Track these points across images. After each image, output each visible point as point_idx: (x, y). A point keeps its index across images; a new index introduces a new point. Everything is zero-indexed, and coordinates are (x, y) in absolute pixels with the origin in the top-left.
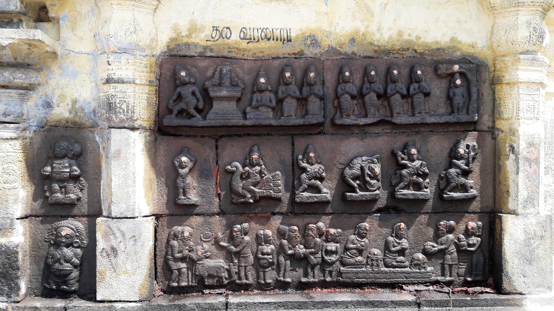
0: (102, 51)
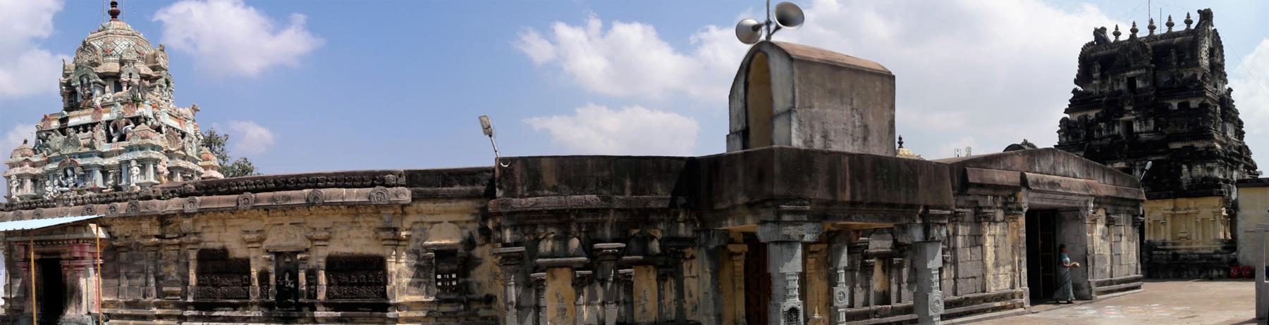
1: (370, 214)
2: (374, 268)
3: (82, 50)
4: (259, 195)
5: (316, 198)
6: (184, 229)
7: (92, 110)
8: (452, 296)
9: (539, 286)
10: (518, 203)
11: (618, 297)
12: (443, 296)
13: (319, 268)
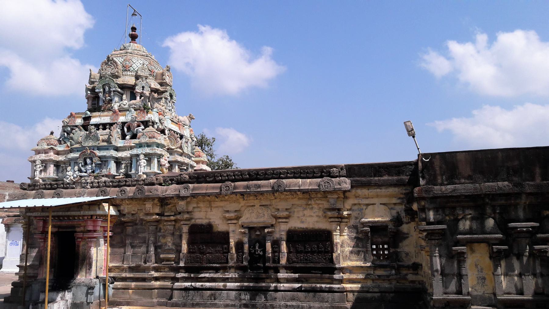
0: (280, 231)
1: (320, 199)
2: (322, 240)
3: (107, 64)
4: (236, 183)
5: (279, 186)
6: (179, 209)
7: (111, 113)
8: (385, 263)
9: (460, 258)
10: (437, 189)
11: (534, 269)
12: (378, 263)
13: (280, 240)
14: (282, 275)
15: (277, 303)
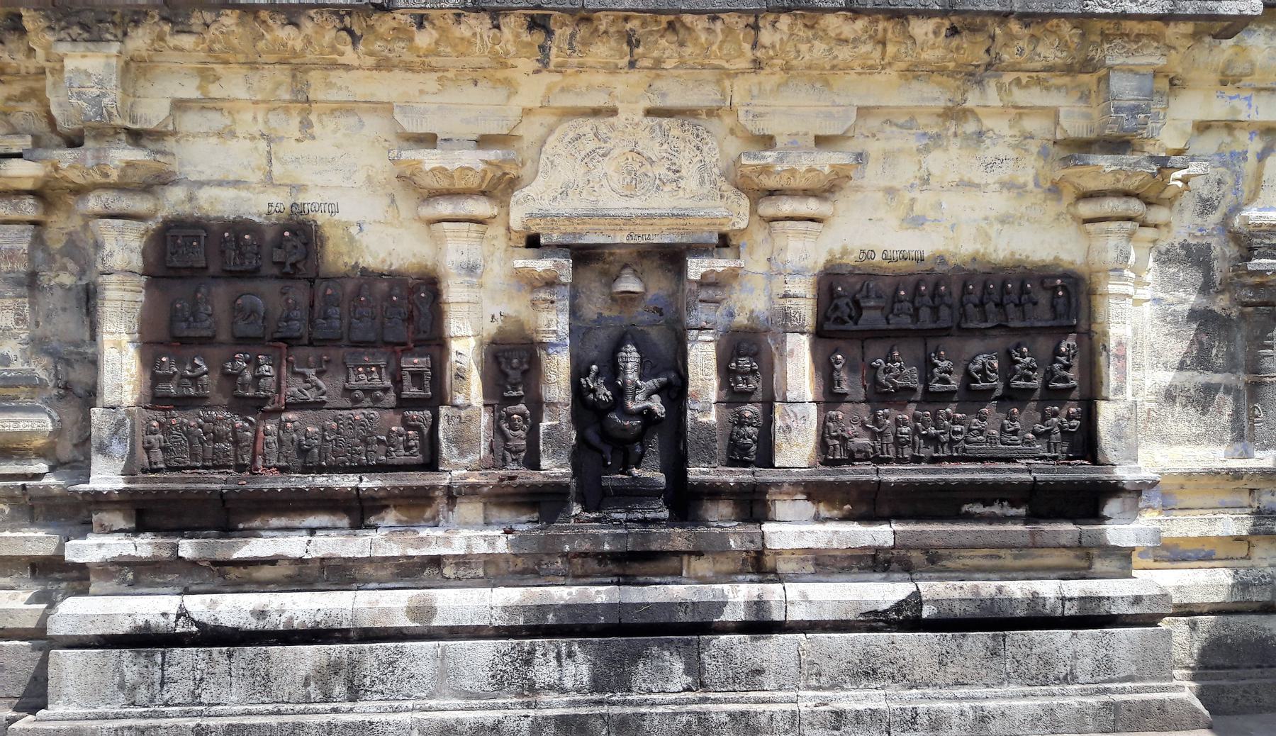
1: (1041, 76)
2: (1050, 310)
6: (66, 106)
13: (784, 322)
14: (793, 529)
15: (771, 703)
